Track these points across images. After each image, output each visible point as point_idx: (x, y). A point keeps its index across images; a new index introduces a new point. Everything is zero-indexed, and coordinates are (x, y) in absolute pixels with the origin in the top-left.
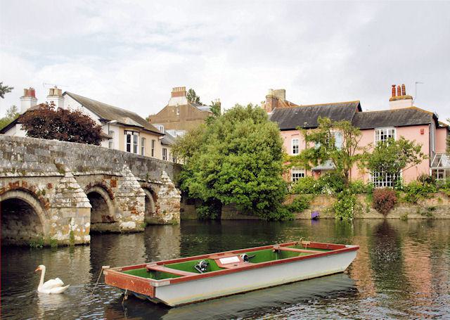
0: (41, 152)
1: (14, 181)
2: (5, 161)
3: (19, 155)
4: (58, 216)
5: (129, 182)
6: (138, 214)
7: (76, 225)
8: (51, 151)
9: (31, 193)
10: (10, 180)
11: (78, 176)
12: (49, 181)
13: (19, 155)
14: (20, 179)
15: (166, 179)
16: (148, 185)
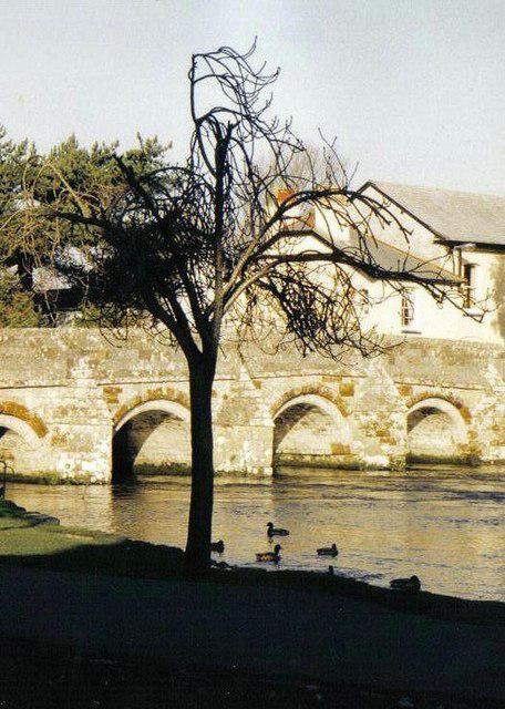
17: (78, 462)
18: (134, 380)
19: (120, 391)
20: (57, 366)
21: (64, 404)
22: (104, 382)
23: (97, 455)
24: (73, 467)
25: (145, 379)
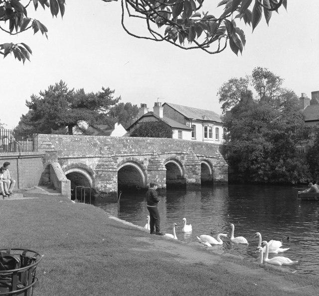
1: (128, 157)
6: (197, 174)
17: (105, 184)
18: (122, 155)
19: (118, 159)
20: (97, 150)
21: (100, 164)
22: (112, 155)
23: (112, 182)
24: (103, 186)
25: (126, 155)
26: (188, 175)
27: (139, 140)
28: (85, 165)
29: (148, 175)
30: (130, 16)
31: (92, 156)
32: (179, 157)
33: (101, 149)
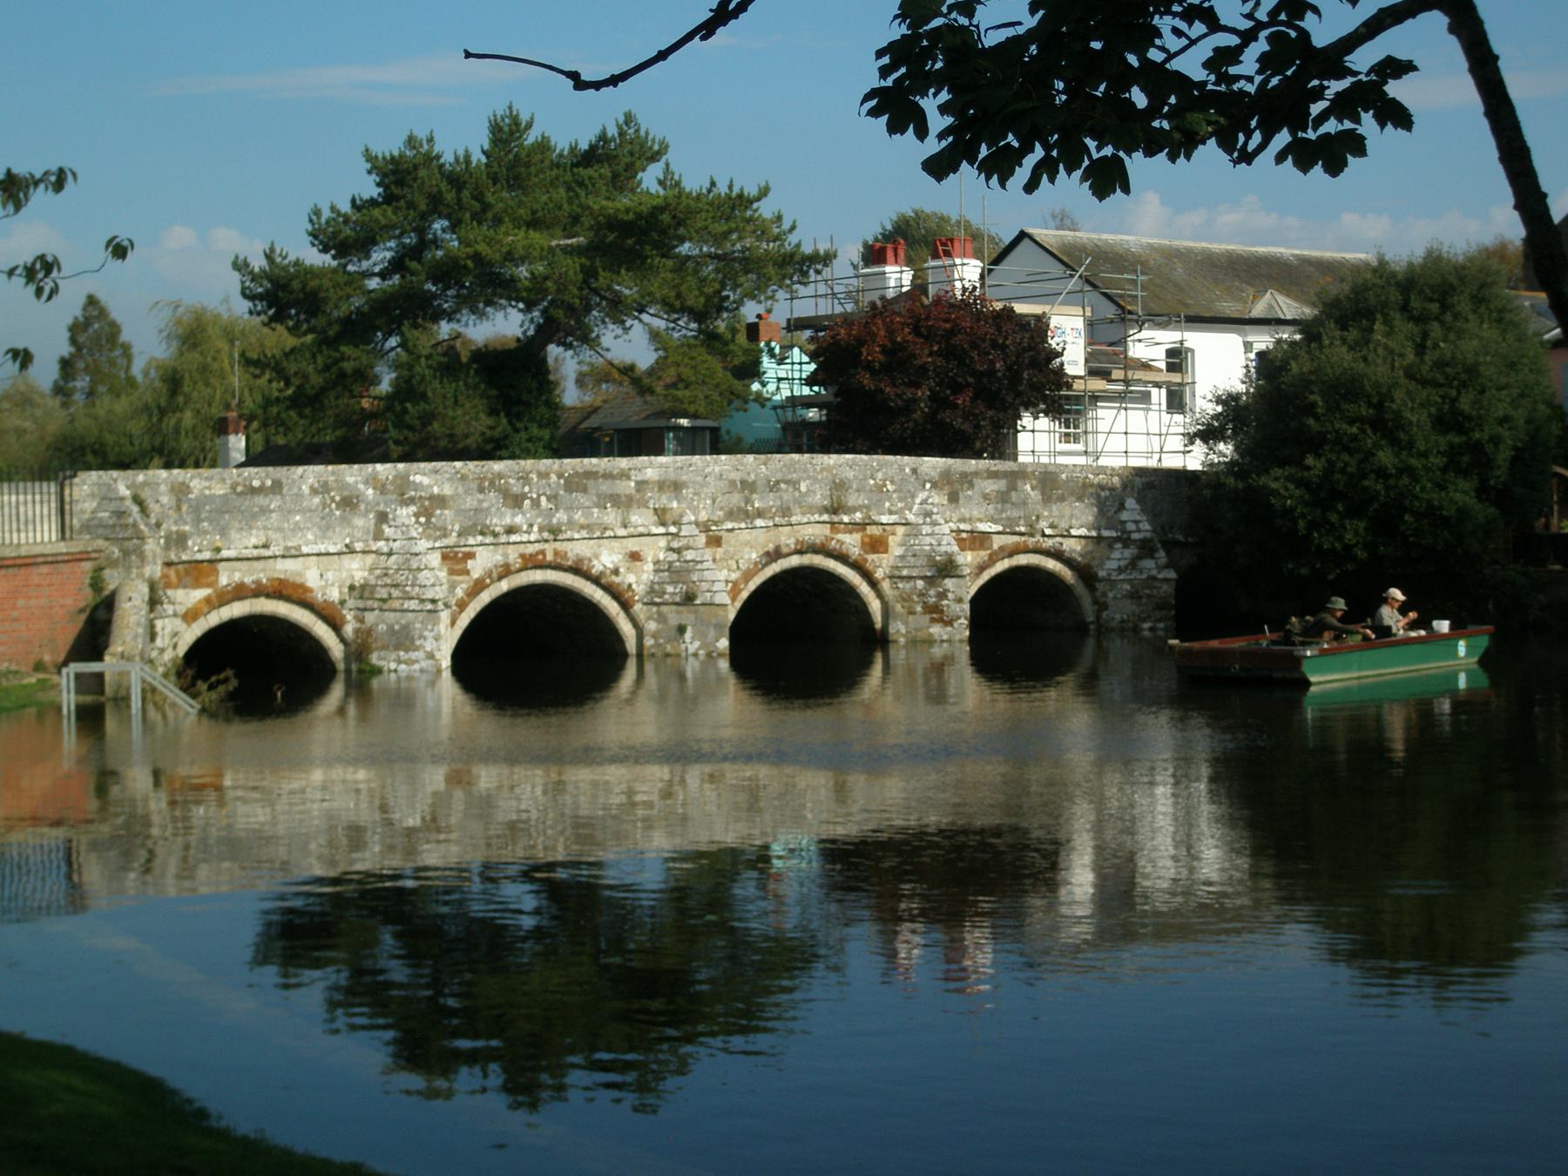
0: (605, 487)
1: (531, 549)
2: (509, 512)
3: (543, 499)
4: (658, 621)
5: (928, 540)
6: (950, 623)
7: (697, 644)
8: (638, 483)
9: (843, 558)
10: (521, 548)
11: (732, 530)
12: (632, 544)
13: (543, 499)
14: (546, 546)
15: (1136, 522)
16: (1049, 543)
26: (906, 623)
27: (591, 475)
28: (308, 590)
29: (652, 626)
30: (1022, 235)
31: (332, 549)
32: (851, 542)
33: (383, 518)
